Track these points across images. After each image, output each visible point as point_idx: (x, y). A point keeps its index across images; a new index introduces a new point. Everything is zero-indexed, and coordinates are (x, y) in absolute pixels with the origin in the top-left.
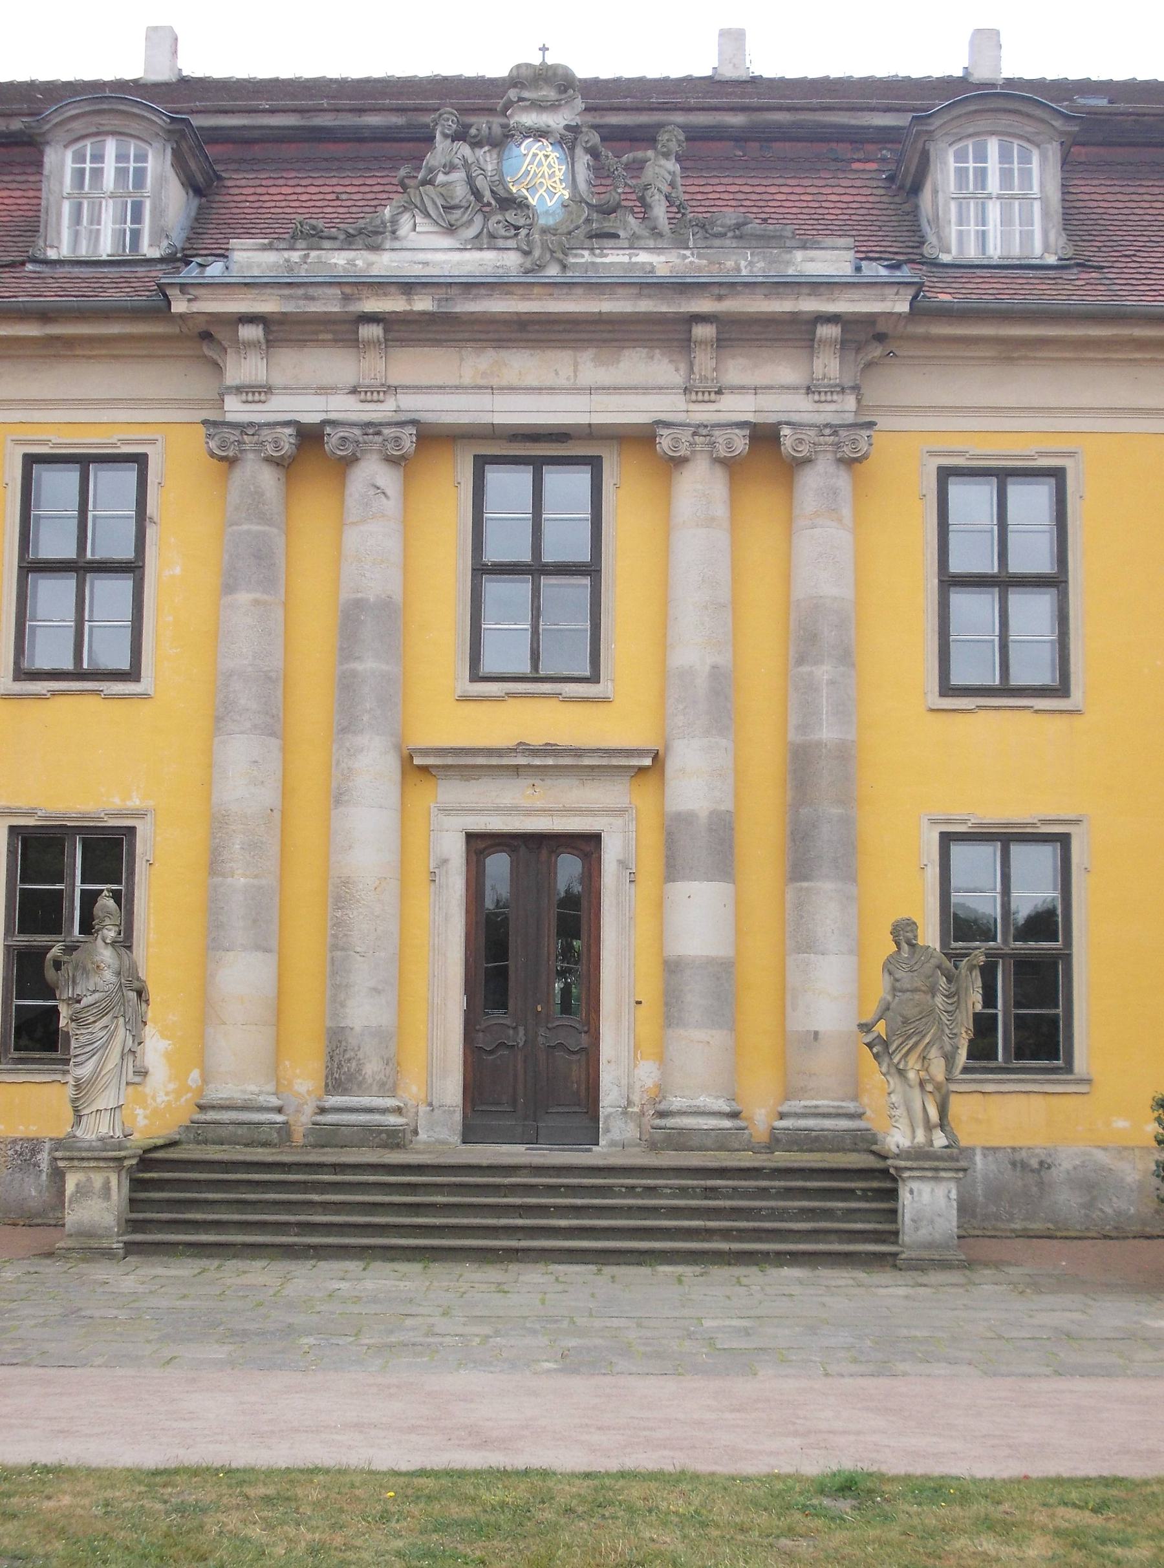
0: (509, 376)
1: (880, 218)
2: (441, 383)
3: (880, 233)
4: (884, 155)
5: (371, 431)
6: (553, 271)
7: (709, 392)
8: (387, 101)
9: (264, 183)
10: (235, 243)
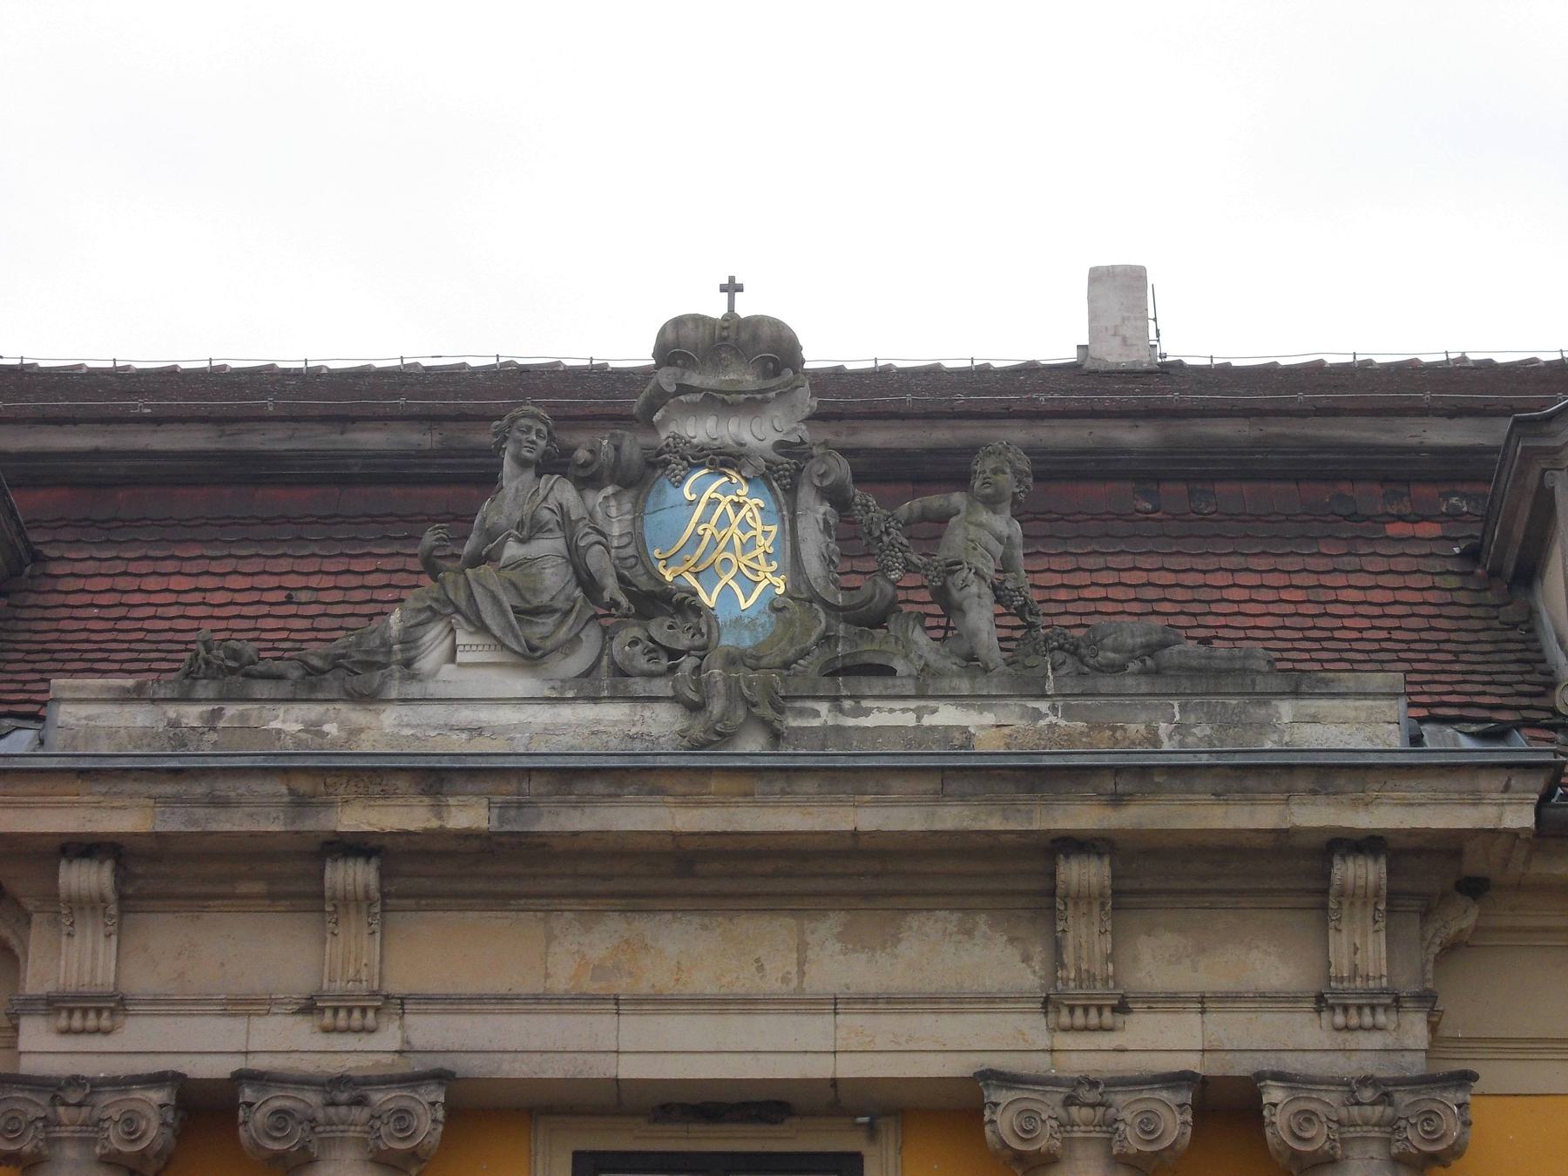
0: (655, 976)
1: (1453, 636)
2: (503, 990)
3: (1457, 667)
4: (1456, 507)
5: (344, 1097)
6: (752, 744)
7: (1100, 1009)
8: (402, 401)
9: (133, 568)
10: (63, 688)
